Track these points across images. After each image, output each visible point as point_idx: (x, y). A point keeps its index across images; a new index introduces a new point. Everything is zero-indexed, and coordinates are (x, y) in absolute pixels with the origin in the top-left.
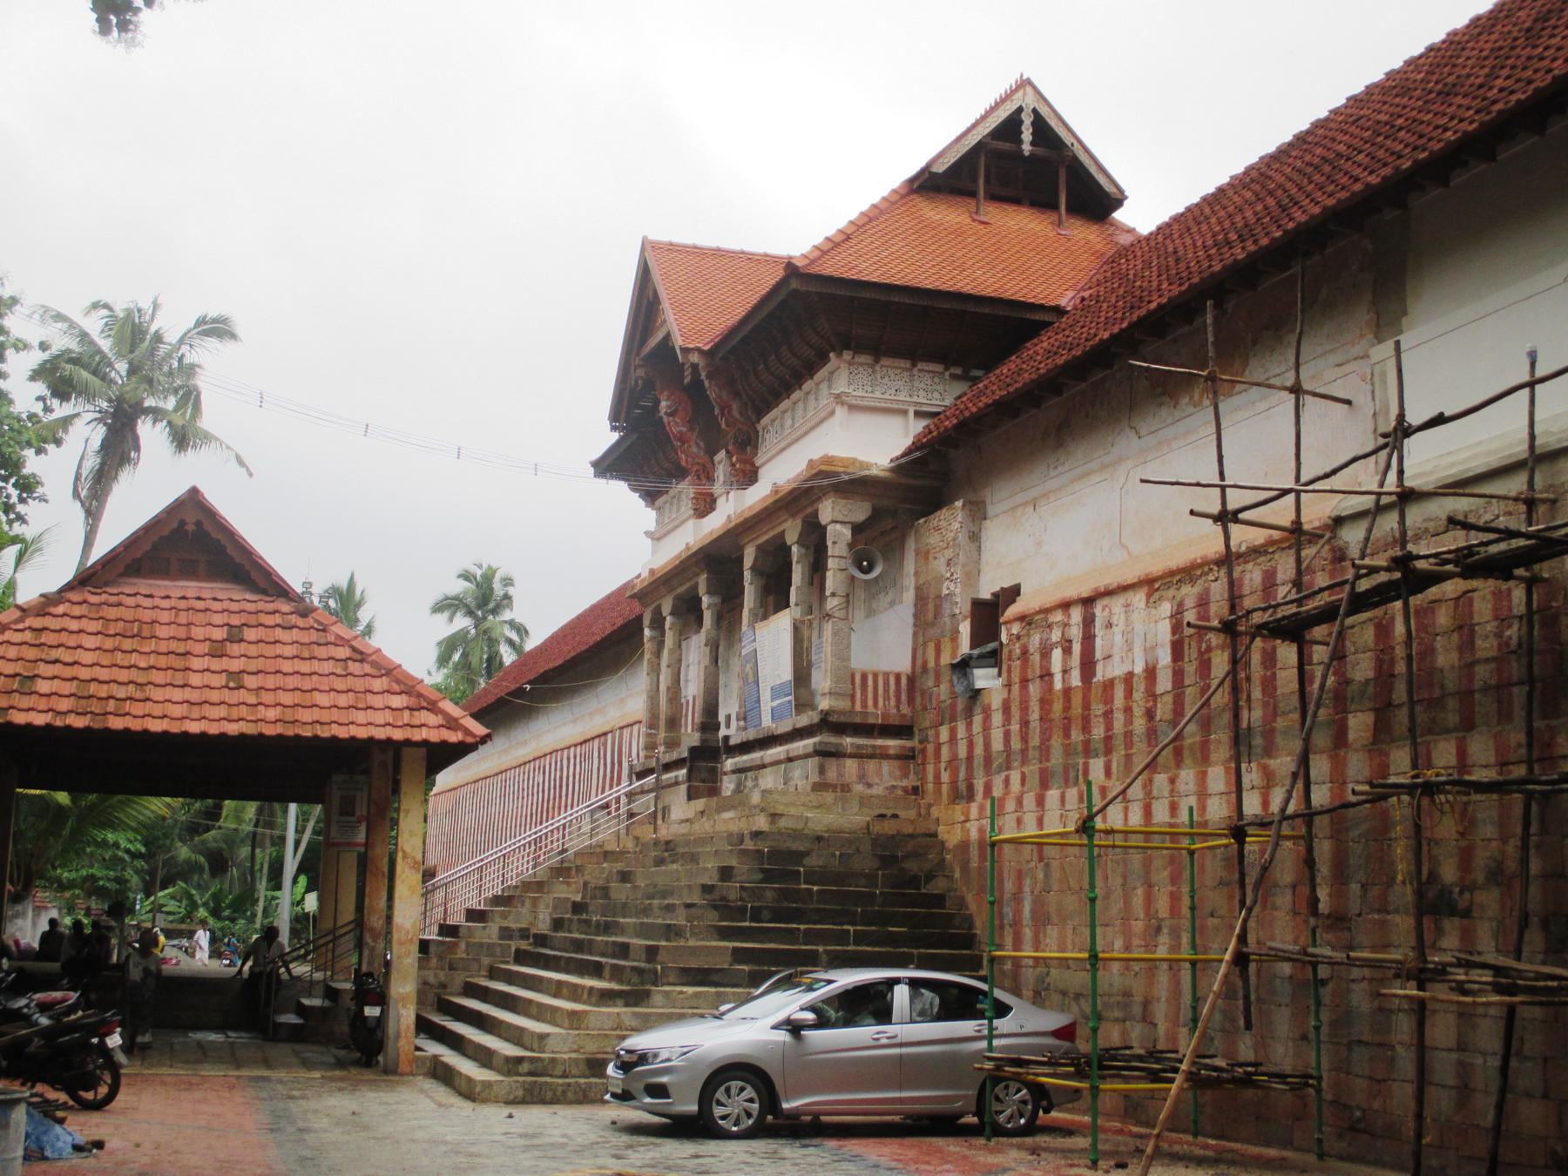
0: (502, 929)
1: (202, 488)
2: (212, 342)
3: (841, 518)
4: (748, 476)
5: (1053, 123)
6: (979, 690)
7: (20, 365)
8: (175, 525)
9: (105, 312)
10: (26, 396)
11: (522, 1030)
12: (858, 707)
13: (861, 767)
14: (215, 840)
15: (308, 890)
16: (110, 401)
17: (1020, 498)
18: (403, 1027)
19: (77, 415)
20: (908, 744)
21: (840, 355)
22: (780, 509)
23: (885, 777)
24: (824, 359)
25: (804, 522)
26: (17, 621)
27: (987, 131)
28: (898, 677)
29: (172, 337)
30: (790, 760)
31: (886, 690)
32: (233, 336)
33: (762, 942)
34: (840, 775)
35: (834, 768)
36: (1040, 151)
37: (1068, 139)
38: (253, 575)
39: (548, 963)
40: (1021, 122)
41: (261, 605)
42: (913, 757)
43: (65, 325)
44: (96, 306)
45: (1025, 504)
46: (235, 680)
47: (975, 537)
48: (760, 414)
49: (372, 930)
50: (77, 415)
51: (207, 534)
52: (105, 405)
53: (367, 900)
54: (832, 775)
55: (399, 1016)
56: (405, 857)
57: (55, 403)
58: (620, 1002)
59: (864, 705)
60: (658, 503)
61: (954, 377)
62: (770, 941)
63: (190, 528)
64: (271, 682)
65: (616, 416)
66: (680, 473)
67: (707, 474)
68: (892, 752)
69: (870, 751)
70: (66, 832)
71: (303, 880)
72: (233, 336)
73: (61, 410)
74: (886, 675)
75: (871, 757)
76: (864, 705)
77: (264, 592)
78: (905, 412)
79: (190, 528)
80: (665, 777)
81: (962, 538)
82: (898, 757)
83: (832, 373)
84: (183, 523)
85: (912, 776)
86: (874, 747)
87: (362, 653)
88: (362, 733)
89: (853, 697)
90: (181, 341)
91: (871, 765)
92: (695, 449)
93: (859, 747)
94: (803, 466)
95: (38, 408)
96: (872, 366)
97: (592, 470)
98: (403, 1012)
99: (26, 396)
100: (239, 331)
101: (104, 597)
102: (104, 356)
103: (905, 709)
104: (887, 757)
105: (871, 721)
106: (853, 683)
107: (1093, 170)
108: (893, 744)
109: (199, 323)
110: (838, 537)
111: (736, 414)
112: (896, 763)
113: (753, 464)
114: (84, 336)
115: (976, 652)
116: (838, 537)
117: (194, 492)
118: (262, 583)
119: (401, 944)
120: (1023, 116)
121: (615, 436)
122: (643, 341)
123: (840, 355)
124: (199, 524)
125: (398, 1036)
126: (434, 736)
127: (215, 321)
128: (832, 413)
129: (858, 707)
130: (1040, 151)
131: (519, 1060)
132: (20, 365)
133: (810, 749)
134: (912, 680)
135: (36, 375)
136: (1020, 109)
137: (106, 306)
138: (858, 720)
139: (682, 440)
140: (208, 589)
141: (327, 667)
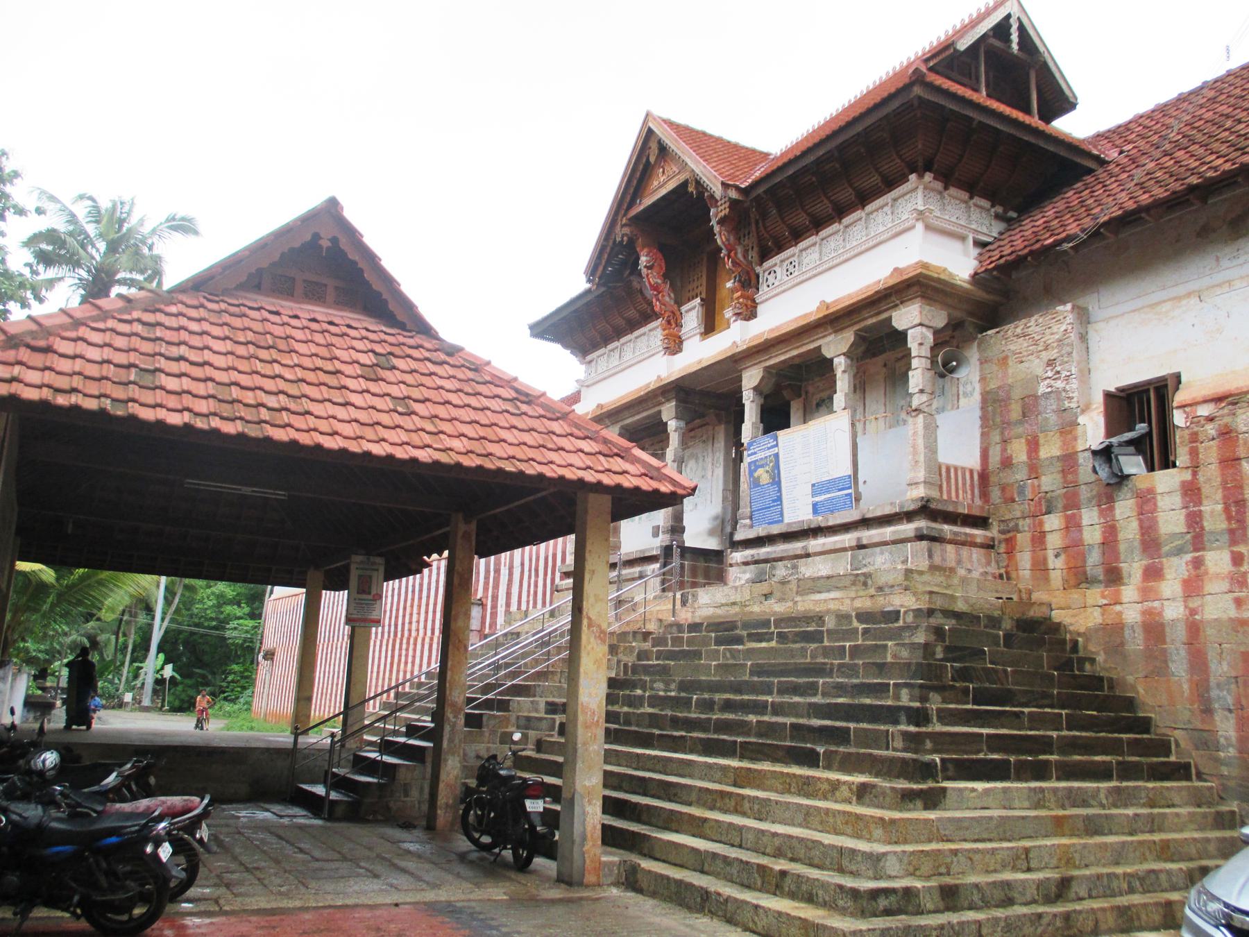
0: (547, 703)
1: (340, 199)
2: (178, 236)
3: (926, 322)
4: (749, 313)
5: (1031, 32)
6: (1129, 476)
7: (18, 229)
8: (308, 237)
9: (90, 203)
10: (19, 260)
11: (741, 829)
12: (945, 497)
13: (958, 554)
14: (93, 628)
15: (166, 662)
16: (89, 271)
17: (1181, 290)
18: (589, 829)
19: (60, 279)
20: (988, 534)
21: (921, 176)
22: (826, 323)
23: (974, 564)
24: (904, 179)
25: (856, 334)
26: (121, 311)
27: (991, 26)
28: (971, 471)
29: (146, 229)
30: (861, 547)
31: (964, 484)
32: (196, 233)
33: (996, 727)
34: (944, 560)
35: (939, 553)
36: (1021, 55)
37: (1042, 49)
38: (392, 306)
39: (646, 741)
40: (1011, 26)
41: (401, 339)
42: (992, 547)
43: (59, 206)
44: (81, 197)
45: (1189, 295)
46: (404, 406)
47: (1083, 338)
48: (765, 255)
49: (454, 705)
50: (60, 279)
51: (342, 254)
52: (84, 274)
53: (449, 674)
54: (937, 560)
55: (584, 813)
56: (590, 626)
57: (41, 268)
58: (919, 803)
59: (949, 492)
60: (589, 358)
61: (997, 217)
62: (1003, 727)
63: (325, 243)
64: (442, 411)
65: (592, 272)
66: (647, 317)
67: (674, 322)
68: (978, 540)
69: (963, 538)
70: (46, 607)
71: (162, 656)
72: (196, 233)
73: (47, 273)
74: (963, 469)
75: (963, 544)
76: (949, 492)
77: (402, 326)
78: (963, 238)
79: (325, 243)
80: (624, 572)
81: (1073, 337)
82: (983, 546)
83: (895, 200)
84: (316, 236)
85: (993, 564)
86: (966, 534)
87: (527, 395)
88: (570, 474)
89: (941, 487)
90: (154, 232)
91: (965, 551)
92: (667, 299)
93: (956, 534)
94: (887, 272)
95: (26, 272)
96: (940, 193)
97: (528, 331)
98: (589, 809)
99: (19, 260)
100: (201, 228)
101: (223, 306)
102: (88, 236)
103: (978, 502)
104: (973, 544)
105: (960, 510)
106: (940, 475)
107: (1057, 75)
108: (978, 534)
109: (168, 220)
110: (919, 343)
111: (740, 256)
112: (982, 551)
113: (754, 301)
114: (73, 219)
115: (1114, 440)
116: (919, 343)
117: (332, 207)
118: (400, 317)
119: (587, 727)
120: (1012, 20)
121: (588, 286)
122: (632, 204)
123: (921, 176)
124: (334, 240)
125: (584, 838)
126: (628, 482)
127: (183, 219)
128: (913, 227)
129: (945, 497)
130: (1021, 55)
131: (875, 894)
132: (18, 229)
133: (912, 534)
134: (984, 477)
135: (31, 242)
136: (1009, 16)
137: (91, 199)
138: (950, 508)
139: (655, 288)
140: (343, 316)
141: (495, 404)
